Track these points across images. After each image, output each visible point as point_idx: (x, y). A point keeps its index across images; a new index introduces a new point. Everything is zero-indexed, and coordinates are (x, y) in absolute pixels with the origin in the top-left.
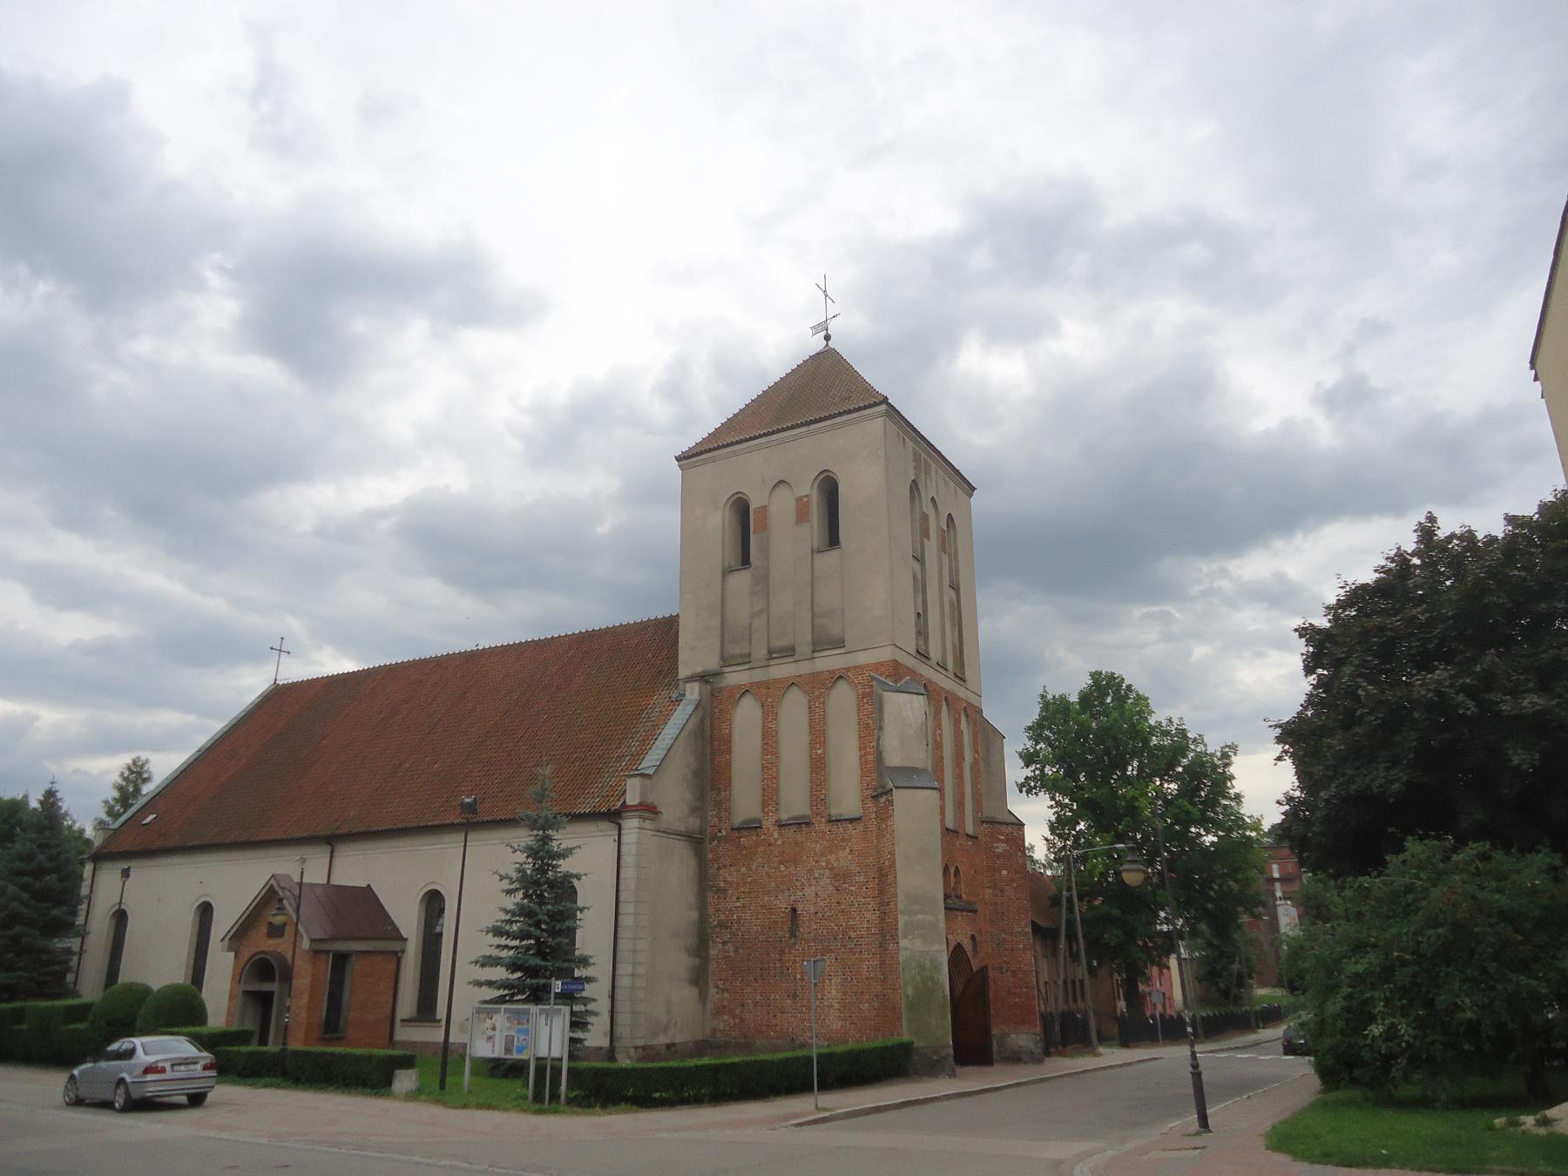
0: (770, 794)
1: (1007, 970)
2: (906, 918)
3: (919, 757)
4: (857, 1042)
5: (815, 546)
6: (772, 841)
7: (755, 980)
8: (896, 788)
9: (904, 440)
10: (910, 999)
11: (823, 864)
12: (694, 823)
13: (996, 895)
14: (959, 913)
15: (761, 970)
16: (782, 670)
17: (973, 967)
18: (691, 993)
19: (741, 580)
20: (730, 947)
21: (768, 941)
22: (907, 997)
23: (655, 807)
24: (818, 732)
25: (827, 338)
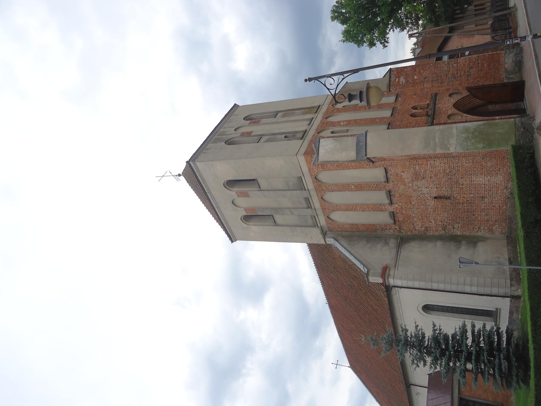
0: (377, 208)
1: (469, 72)
2: (438, 148)
3: (351, 142)
4: (510, 167)
5: (258, 189)
6: (400, 207)
7: (474, 215)
8: (366, 155)
9: (207, 149)
10: (485, 145)
11: (410, 185)
12: (392, 243)
13: (428, 81)
14: (437, 106)
15: (468, 212)
16: (316, 203)
17: (467, 94)
18: (481, 247)
19: (279, 218)
20: (456, 226)
21: (452, 209)
22: (484, 147)
23: (384, 267)
24: (344, 187)
25: (179, 175)
